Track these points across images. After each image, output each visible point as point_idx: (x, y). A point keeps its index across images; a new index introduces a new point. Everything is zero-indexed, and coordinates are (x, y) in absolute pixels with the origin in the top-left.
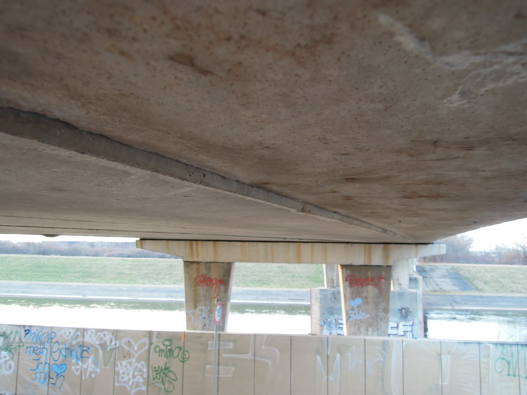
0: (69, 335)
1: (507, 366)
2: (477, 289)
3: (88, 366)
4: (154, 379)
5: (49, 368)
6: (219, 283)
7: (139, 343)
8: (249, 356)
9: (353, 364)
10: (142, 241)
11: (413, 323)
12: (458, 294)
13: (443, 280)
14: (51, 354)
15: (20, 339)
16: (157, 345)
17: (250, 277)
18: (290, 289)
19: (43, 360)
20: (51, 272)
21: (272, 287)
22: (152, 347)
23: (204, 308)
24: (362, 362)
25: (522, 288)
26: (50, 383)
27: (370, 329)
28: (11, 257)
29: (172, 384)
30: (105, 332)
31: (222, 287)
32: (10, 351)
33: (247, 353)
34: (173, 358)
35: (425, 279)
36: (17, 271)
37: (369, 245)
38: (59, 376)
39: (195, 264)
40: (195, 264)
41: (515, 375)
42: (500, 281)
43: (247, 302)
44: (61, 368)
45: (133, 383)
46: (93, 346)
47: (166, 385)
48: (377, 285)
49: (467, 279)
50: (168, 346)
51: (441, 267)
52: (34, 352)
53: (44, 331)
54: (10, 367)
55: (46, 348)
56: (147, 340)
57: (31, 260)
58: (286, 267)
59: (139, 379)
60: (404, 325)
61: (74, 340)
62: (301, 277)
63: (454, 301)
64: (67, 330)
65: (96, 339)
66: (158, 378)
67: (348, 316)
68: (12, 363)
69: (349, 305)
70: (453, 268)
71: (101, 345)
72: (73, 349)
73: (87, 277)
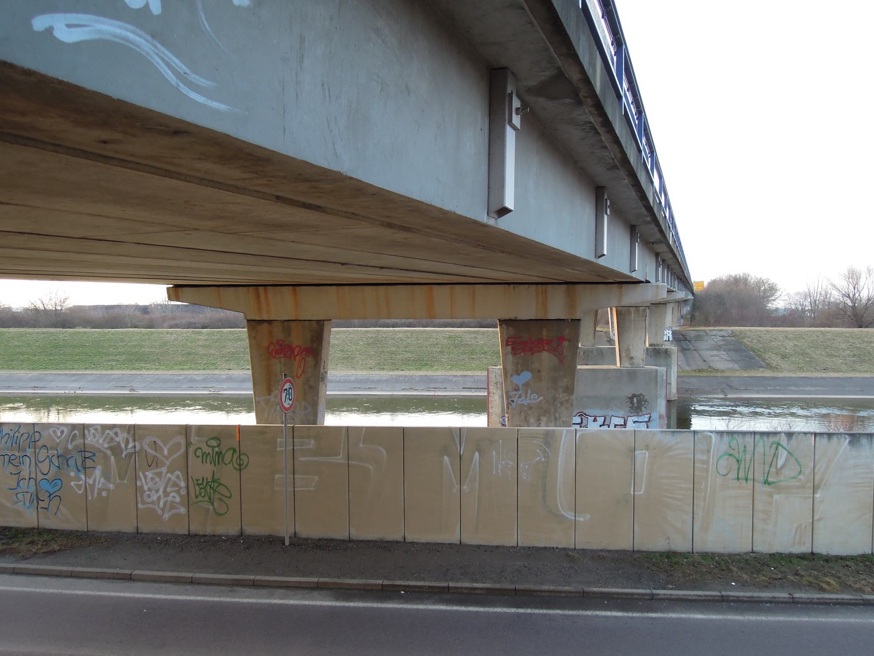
0: (61, 436)
1: (735, 466)
2: (769, 366)
3: (94, 481)
4: (196, 497)
5: (36, 485)
7: (168, 446)
8: (340, 459)
10: (177, 289)
11: (650, 417)
12: (737, 374)
13: (715, 352)
14: (36, 464)
17: (402, 354)
18: (465, 373)
19: (25, 473)
20: (76, 355)
21: (437, 370)
22: (191, 450)
25: (842, 363)
27: (544, 419)
28: (9, 332)
31: (310, 360)
33: (337, 454)
34: (223, 465)
35: (686, 351)
36: (22, 354)
37: (544, 286)
38: (52, 497)
39: (265, 325)
41: (747, 480)
42: (808, 354)
43: (395, 393)
45: (165, 503)
46: (100, 451)
48: (556, 351)
49: (754, 352)
50: (215, 447)
51: (714, 333)
53: (22, 430)
55: (28, 456)
56: (182, 440)
57: (43, 336)
58: (460, 337)
59: (174, 497)
60: (635, 422)
62: (485, 353)
63: (728, 385)
65: (104, 441)
66: (203, 494)
67: (509, 400)
70: (733, 334)
71: (111, 448)
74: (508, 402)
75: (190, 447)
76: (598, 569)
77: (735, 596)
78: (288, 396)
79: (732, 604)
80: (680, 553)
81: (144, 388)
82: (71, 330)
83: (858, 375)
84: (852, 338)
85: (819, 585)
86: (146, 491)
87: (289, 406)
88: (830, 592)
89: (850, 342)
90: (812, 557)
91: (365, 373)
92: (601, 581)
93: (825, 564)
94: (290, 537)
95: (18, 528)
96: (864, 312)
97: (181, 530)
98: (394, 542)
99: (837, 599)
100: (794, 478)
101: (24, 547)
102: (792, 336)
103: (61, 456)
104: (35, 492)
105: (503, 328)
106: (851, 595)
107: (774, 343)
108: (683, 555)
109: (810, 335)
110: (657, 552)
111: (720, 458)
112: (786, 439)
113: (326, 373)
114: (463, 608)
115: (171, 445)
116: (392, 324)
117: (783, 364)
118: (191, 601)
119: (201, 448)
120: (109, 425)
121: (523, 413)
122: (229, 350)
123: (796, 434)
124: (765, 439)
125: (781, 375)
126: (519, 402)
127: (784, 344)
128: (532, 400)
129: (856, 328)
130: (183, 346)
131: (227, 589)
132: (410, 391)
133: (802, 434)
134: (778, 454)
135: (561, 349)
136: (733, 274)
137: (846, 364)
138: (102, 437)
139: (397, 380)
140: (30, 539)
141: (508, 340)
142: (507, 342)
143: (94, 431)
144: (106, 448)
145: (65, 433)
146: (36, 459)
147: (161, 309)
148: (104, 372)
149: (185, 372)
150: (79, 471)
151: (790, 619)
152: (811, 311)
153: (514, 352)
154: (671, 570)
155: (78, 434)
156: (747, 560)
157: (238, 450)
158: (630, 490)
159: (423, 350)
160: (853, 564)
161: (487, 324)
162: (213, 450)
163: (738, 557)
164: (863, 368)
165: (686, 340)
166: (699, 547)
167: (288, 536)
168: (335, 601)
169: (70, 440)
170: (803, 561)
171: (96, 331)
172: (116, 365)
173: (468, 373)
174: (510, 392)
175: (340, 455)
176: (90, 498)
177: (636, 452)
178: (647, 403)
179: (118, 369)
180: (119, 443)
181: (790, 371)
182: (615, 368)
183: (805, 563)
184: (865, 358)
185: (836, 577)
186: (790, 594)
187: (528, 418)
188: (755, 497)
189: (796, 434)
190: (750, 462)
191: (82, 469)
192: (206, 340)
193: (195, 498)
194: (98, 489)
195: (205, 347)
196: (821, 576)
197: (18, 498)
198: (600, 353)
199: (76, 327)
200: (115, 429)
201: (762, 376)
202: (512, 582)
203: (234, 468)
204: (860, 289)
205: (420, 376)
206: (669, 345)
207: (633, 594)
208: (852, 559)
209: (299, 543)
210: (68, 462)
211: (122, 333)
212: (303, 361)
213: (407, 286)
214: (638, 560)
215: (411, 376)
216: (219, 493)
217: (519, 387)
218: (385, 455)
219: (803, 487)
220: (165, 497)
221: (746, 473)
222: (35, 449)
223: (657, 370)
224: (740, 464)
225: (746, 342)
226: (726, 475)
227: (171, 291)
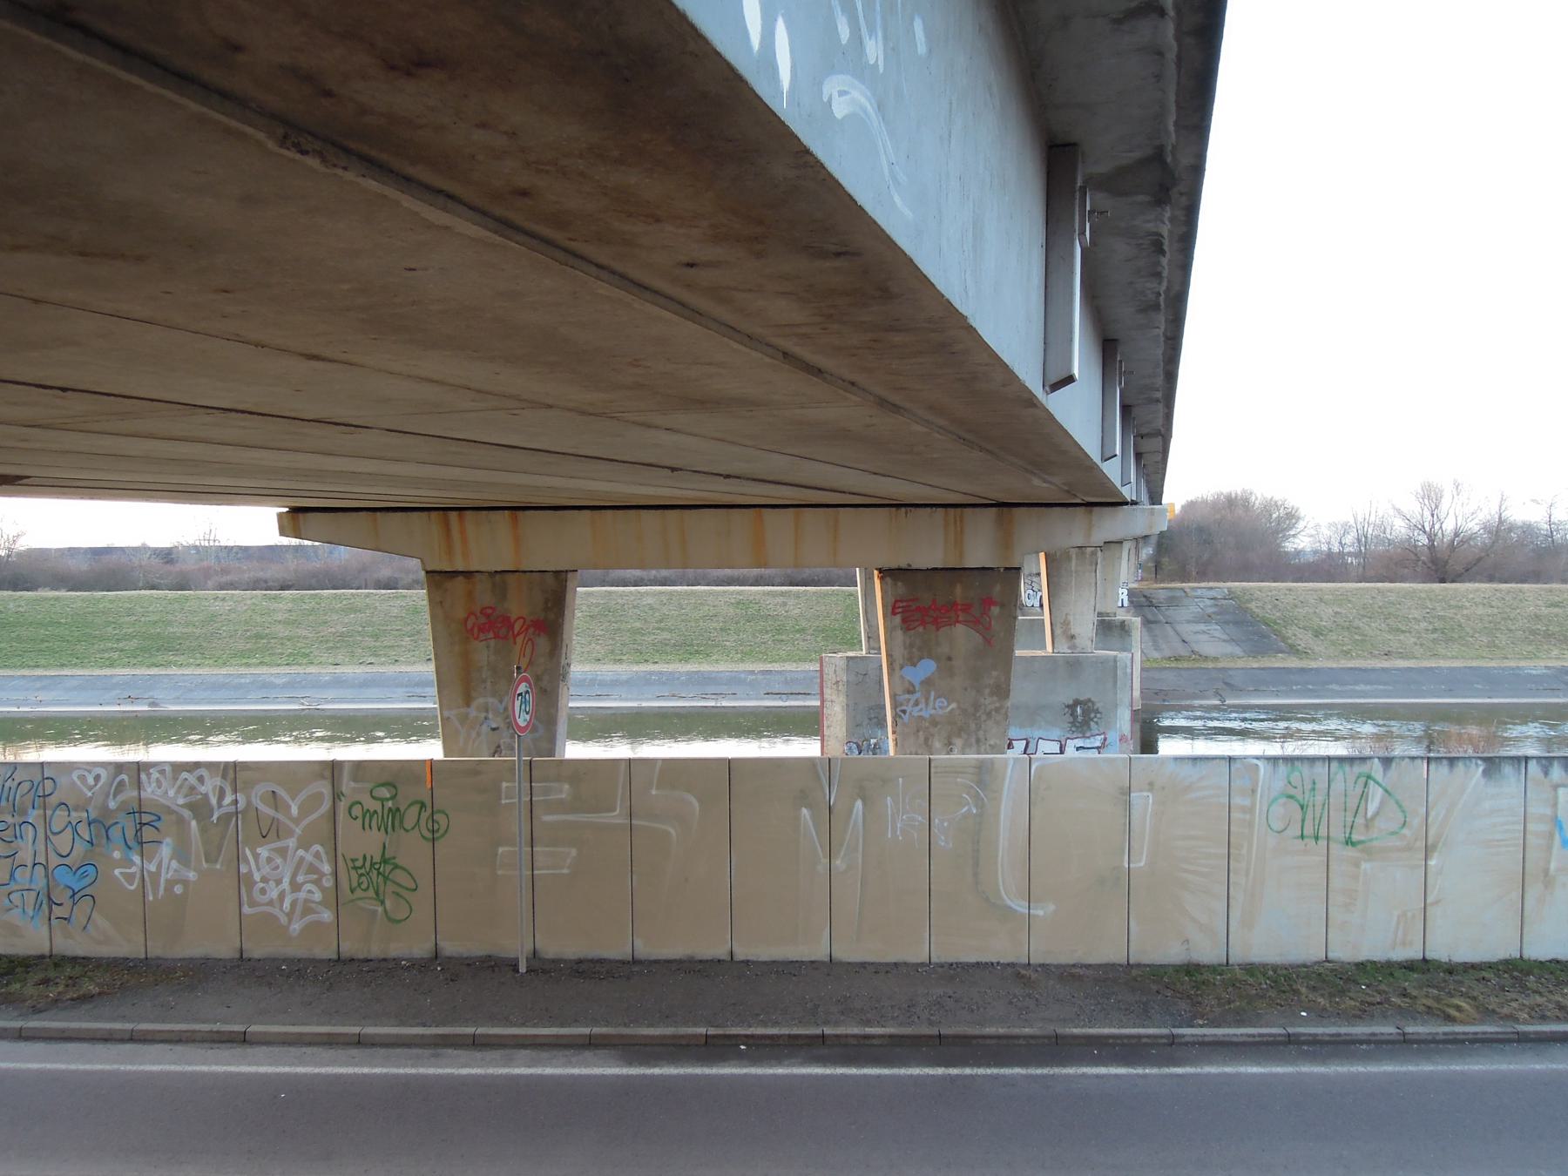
0: (96, 785)
1: (1298, 815)
2: (1293, 650)
3: (159, 866)
4: (352, 891)
5: (47, 876)
6: (531, 630)
7: (302, 796)
8: (616, 817)
11: (1105, 739)
12: (1240, 664)
13: (1202, 627)
14: (47, 837)
16: (357, 798)
17: (654, 634)
18: (769, 667)
19: (26, 855)
22: (343, 806)
23: (491, 700)
25: (1416, 644)
27: (958, 742)
30: (204, 772)
31: (542, 642)
35: (1153, 626)
37: (959, 510)
38: (77, 897)
40: (460, 578)
41: (1317, 838)
43: (644, 704)
45: (294, 904)
46: (170, 811)
47: (388, 903)
48: (978, 623)
49: (1267, 624)
50: (388, 800)
51: (1199, 592)
53: (18, 777)
55: (31, 824)
56: (324, 788)
59: (310, 891)
60: (1078, 749)
61: (111, 797)
62: (803, 631)
63: (1226, 683)
64: (90, 772)
65: (178, 792)
66: (363, 887)
67: (898, 710)
70: (1231, 595)
71: (190, 806)
72: (112, 822)
73: (158, 650)
74: (896, 714)
75: (341, 801)
76: (1073, 997)
77: (1310, 1035)
78: (523, 707)
79: (1306, 1048)
80: (1208, 967)
81: (177, 701)
82: (30, 593)
83: (1443, 664)
84: (1431, 600)
85: (1444, 1012)
86: (256, 883)
87: (526, 723)
88: (1463, 1022)
89: (1427, 608)
90: (1423, 966)
92: (1082, 1018)
93: (1447, 977)
94: (527, 958)
95: (14, 956)
96: (1449, 556)
97: (325, 951)
98: (712, 961)
99: (1476, 1033)
100: (1393, 833)
101: (30, 990)
102: (1331, 597)
103: (95, 821)
104: (46, 890)
105: (887, 583)
106: (1498, 1026)
107: (1300, 610)
108: (1214, 969)
109: (1361, 595)
110: (1169, 965)
111: (1273, 802)
112: (1382, 769)
113: (569, 665)
114: (853, 1071)
115: (304, 797)
117: (1318, 645)
118: (365, 1075)
119: (360, 803)
120: (187, 763)
121: (921, 733)
122: (333, 630)
123: (1398, 760)
124: (1347, 768)
125: (1313, 665)
126: (915, 714)
127: (1317, 611)
129: (1436, 582)
130: (246, 622)
131: (427, 1052)
132: (670, 700)
133: (1407, 760)
135: (988, 619)
136: (1225, 491)
137: (1421, 645)
138: (174, 784)
139: (646, 681)
140: (40, 976)
142: (894, 608)
143: (158, 775)
144: (181, 806)
145: (103, 780)
146: (46, 827)
147: (197, 553)
148: (97, 672)
149: (253, 670)
150: (130, 848)
151: (1404, 1069)
152: (1357, 555)
153: (907, 624)
154: (1197, 995)
156: (1320, 974)
157: (429, 805)
158: (1123, 861)
159: (691, 627)
160: (1493, 976)
161: (803, 579)
162: (383, 806)
163: (1305, 970)
164: (1450, 652)
165: (1151, 605)
166: (1238, 956)
167: (525, 956)
168: (626, 1067)
170: (1411, 973)
171: (78, 596)
172: (120, 658)
173: (773, 667)
175: (615, 810)
176: (151, 898)
177: (1132, 795)
178: (1098, 715)
179: (124, 666)
181: (1329, 658)
182: (1043, 654)
183: (1415, 976)
184: (1453, 635)
185: (1469, 997)
186: (1398, 1028)
187: (930, 740)
188: (1330, 867)
189: (1398, 760)
190: (1323, 809)
194: (167, 880)
196: (1443, 997)
197: (11, 902)
199: (40, 589)
200: (199, 770)
201: (1282, 666)
202: (931, 1023)
204: (1442, 516)
206: (1124, 614)
207: (1139, 1037)
208: (1490, 967)
209: (543, 968)
211: (129, 598)
212: (530, 642)
213: (743, 510)
214: (1139, 979)
216: (394, 882)
217: (913, 686)
218: (698, 809)
219: (1409, 848)
221: (1316, 827)
222: (45, 810)
223: (1116, 657)
224: (1306, 812)
225: (1253, 607)
226: (1282, 831)
227: (286, 522)
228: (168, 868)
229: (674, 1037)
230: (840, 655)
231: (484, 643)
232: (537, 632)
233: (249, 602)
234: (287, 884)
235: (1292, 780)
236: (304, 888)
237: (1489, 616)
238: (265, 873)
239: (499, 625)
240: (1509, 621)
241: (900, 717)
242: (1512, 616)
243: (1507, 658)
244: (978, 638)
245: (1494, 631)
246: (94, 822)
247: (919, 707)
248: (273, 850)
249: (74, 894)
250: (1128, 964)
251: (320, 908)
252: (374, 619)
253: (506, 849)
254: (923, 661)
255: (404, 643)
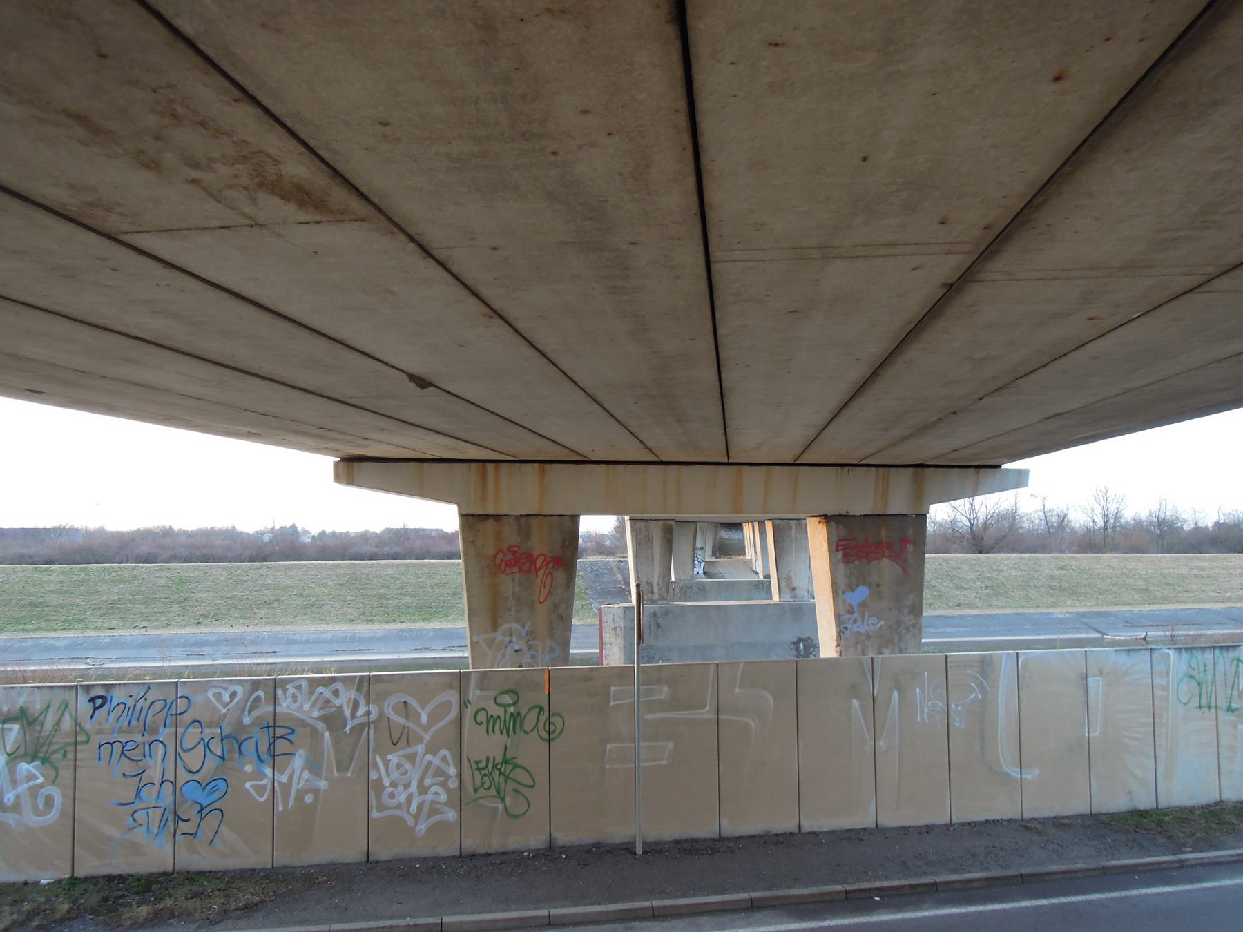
0: (231, 702)
3: (291, 777)
4: (476, 790)
5: (174, 792)
6: (551, 565)
7: (429, 707)
8: (707, 713)
9: (925, 710)
14: (176, 755)
15: (76, 723)
16: (482, 705)
19: (155, 774)
22: (468, 713)
23: (515, 626)
24: (941, 704)
25: (976, 597)
26: (178, 833)
29: (522, 795)
30: (339, 686)
31: (560, 575)
32: (44, 760)
33: (703, 707)
37: (887, 469)
38: (204, 813)
39: (491, 522)
40: (491, 521)
41: (1209, 707)
43: (402, 656)
44: (215, 789)
46: (303, 723)
47: (508, 800)
48: (895, 557)
50: (510, 705)
52: (124, 754)
53: (151, 697)
54: (49, 802)
56: (452, 696)
59: (436, 793)
61: (246, 712)
64: (226, 689)
65: (313, 706)
66: (486, 786)
67: (842, 626)
68: (56, 793)
69: (844, 601)
71: (325, 719)
74: (840, 631)
75: (467, 708)
83: (997, 611)
84: (979, 565)
89: (978, 571)
91: (344, 627)
97: (447, 848)
98: (785, 834)
103: (228, 737)
104: (172, 807)
105: (831, 526)
116: (368, 555)
119: (484, 709)
126: (854, 630)
128: (871, 626)
134: (1239, 672)
137: (980, 598)
139: (399, 637)
141: (838, 543)
142: (837, 545)
144: (316, 719)
149: (31, 635)
150: (262, 761)
153: (847, 559)
155: (263, 697)
159: (429, 592)
166: (1163, 803)
169: (247, 708)
174: (842, 615)
175: (705, 707)
176: (281, 809)
180: (340, 708)
191: (269, 756)
192: (61, 582)
193: (473, 793)
194: (298, 791)
195: (61, 593)
198: (702, 588)
203: (541, 738)
205: (434, 630)
210: (241, 748)
212: (549, 576)
215: (419, 630)
216: (514, 780)
217: (853, 608)
218: (772, 701)
220: (420, 795)
228: (299, 779)
229: (821, 894)
230: (616, 606)
231: (510, 576)
232: (556, 567)
233: (20, 574)
234: (415, 788)
235: (1192, 664)
236: (430, 790)
237: (1020, 576)
238: (393, 779)
239: (524, 561)
240: (1035, 581)
241: (843, 632)
242: (1036, 576)
243: (1039, 607)
244: (899, 570)
245: (1026, 587)
246: (228, 738)
247: (857, 624)
248: (402, 756)
249: (202, 809)
250: (1091, 814)
251: (446, 808)
252: (143, 589)
253: (614, 745)
254: (859, 588)
255: (172, 609)
